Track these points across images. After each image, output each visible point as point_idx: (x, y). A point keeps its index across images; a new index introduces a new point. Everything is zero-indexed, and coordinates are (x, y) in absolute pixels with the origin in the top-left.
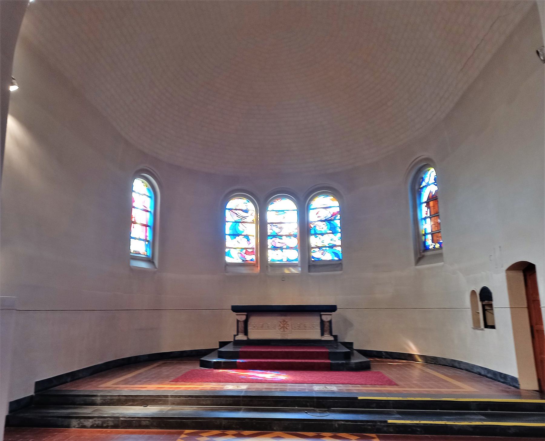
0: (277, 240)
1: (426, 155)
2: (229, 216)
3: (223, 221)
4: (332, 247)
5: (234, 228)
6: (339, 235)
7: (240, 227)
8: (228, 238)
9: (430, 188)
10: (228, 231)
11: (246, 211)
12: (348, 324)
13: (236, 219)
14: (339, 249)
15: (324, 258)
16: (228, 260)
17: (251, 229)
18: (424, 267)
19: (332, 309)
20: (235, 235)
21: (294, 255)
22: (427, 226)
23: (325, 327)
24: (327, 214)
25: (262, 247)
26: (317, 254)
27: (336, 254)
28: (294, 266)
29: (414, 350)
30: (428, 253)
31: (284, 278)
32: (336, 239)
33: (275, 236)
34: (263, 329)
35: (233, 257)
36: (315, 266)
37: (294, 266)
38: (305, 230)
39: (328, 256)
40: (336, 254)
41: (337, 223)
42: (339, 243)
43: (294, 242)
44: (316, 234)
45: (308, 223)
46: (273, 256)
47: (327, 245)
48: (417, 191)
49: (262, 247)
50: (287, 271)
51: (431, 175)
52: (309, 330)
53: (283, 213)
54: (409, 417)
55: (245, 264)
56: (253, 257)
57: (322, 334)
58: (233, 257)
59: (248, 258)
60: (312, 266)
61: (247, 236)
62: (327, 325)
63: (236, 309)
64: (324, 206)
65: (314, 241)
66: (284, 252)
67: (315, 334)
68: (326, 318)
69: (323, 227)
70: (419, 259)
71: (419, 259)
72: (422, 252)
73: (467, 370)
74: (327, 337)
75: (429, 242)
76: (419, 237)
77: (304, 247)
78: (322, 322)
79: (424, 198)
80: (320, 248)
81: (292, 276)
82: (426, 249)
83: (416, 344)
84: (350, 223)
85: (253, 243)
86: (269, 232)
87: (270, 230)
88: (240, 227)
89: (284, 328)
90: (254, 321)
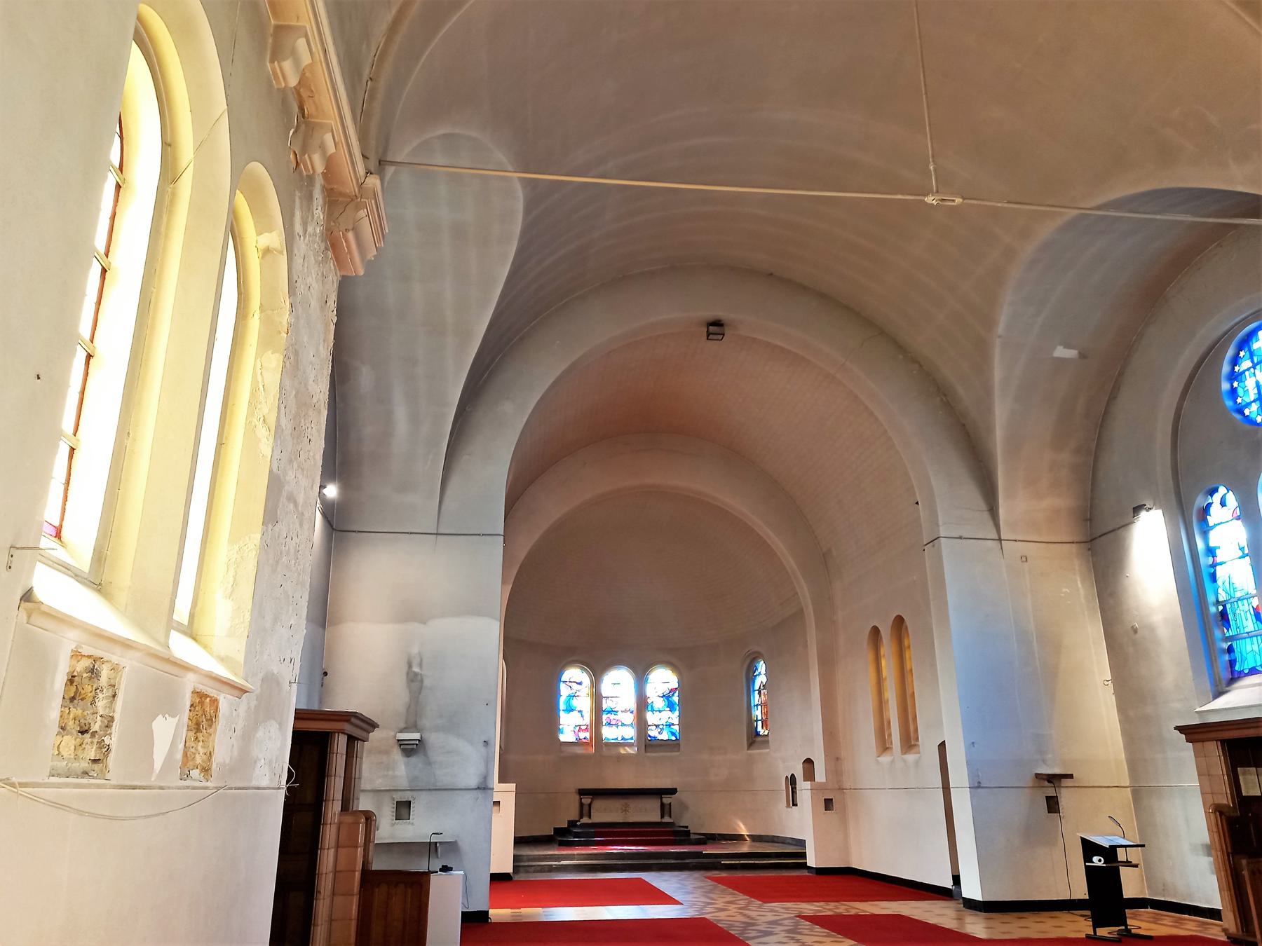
0: (612, 717)
1: (756, 648)
2: (564, 691)
3: (557, 693)
4: (670, 725)
5: (568, 703)
6: (677, 713)
7: (575, 702)
8: (562, 714)
9: (761, 679)
10: (562, 706)
11: (580, 684)
12: (684, 807)
13: (570, 692)
14: (677, 728)
15: (660, 737)
16: (563, 738)
17: (584, 703)
18: (754, 752)
19: (673, 791)
20: (570, 709)
21: (630, 733)
22: (757, 713)
23: (665, 810)
24: (665, 689)
25: (597, 723)
26: (653, 732)
27: (673, 734)
28: (630, 745)
29: (744, 831)
30: (759, 739)
31: (620, 758)
32: (674, 717)
33: (609, 712)
34: (605, 813)
35: (567, 736)
36: (651, 746)
37: (630, 745)
38: (643, 704)
39: (665, 736)
40: (673, 734)
41: (675, 699)
42: (676, 721)
43: (629, 718)
44: (653, 710)
45: (646, 698)
46: (608, 733)
47: (664, 723)
48: (751, 678)
49: (597, 723)
50: (622, 752)
51: (761, 667)
52: (647, 812)
53: (619, 684)
54: (1216, 836)
55: (579, 743)
56: (587, 735)
57: (662, 817)
58: (567, 736)
59: (582, 735)
60: (648, 744)
61: (580, 711)
62: (667, 808)
63: (582, 792)
64: (663, 679)
65: (651, 718)
66: (620, 731)
67: (655, 817)
68: (666, 800)
69: (659, 703)
70: (751, 744)
71: (751, 744)
72: (754, 738)
73: (1113, 397)
74: (667, 819)
75: (759, 728)
76: (751, 723)
77: (641, 725)
78: (662, 805)
79: (757, 687)
80: (657, 726)
81: (629, 756)
82: (757, 734)
83: (745, 824)
84: (689, 700)
85: (587, 720)
86: (605, 707)
87: (606, 705)
88: (575, 702)
89: (625, 811)
90: (599, 804)
